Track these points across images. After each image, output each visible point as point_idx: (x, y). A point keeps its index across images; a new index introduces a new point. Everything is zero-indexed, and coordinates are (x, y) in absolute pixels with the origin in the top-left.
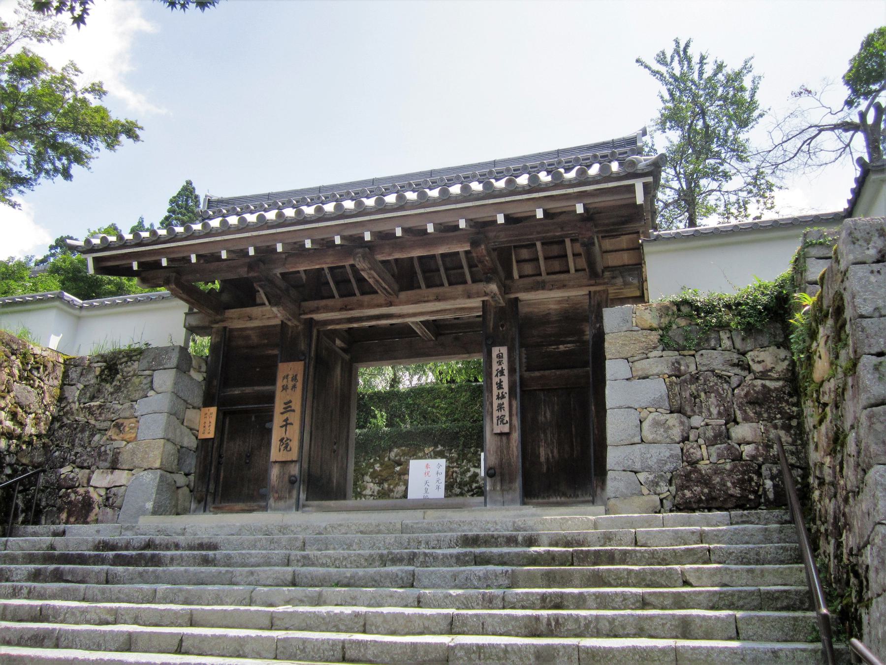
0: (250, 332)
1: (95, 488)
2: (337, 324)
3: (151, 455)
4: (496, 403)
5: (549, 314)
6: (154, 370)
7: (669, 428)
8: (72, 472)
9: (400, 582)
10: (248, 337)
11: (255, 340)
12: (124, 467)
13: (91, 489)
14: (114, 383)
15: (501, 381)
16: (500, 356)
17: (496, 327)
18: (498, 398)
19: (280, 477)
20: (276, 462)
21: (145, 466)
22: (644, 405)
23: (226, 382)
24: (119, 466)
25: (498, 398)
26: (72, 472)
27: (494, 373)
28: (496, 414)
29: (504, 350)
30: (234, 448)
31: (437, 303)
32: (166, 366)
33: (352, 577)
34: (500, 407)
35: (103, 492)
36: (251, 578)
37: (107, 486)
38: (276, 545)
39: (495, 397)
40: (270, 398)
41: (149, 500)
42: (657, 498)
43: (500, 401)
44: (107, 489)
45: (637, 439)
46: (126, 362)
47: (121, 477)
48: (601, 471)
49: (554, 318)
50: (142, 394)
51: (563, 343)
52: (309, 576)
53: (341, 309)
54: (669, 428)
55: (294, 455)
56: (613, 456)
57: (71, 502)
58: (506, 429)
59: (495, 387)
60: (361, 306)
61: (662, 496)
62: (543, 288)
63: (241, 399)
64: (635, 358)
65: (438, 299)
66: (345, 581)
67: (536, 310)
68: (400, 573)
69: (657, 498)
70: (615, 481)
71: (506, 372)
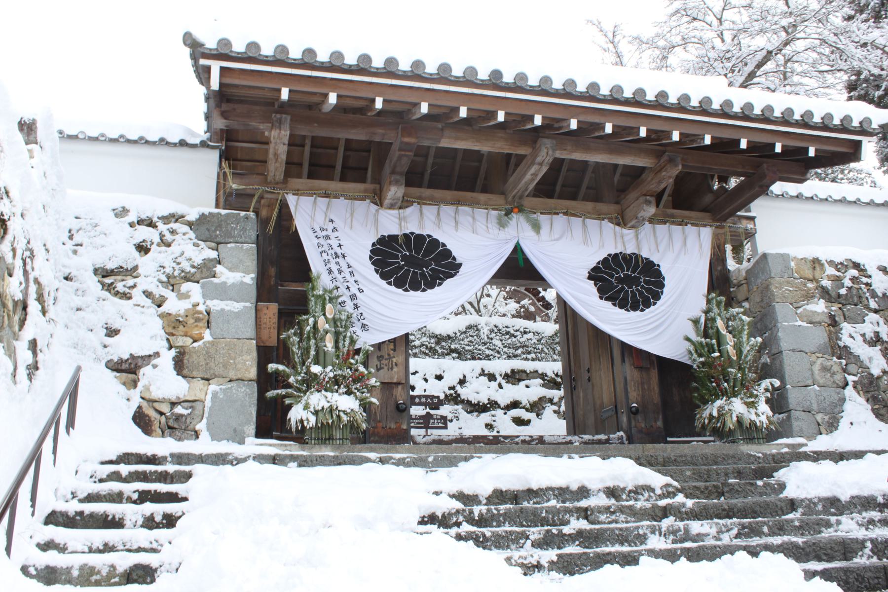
6: (218, 243)
21: (232, 374)
41: (248, 423)
54: (834, 373)
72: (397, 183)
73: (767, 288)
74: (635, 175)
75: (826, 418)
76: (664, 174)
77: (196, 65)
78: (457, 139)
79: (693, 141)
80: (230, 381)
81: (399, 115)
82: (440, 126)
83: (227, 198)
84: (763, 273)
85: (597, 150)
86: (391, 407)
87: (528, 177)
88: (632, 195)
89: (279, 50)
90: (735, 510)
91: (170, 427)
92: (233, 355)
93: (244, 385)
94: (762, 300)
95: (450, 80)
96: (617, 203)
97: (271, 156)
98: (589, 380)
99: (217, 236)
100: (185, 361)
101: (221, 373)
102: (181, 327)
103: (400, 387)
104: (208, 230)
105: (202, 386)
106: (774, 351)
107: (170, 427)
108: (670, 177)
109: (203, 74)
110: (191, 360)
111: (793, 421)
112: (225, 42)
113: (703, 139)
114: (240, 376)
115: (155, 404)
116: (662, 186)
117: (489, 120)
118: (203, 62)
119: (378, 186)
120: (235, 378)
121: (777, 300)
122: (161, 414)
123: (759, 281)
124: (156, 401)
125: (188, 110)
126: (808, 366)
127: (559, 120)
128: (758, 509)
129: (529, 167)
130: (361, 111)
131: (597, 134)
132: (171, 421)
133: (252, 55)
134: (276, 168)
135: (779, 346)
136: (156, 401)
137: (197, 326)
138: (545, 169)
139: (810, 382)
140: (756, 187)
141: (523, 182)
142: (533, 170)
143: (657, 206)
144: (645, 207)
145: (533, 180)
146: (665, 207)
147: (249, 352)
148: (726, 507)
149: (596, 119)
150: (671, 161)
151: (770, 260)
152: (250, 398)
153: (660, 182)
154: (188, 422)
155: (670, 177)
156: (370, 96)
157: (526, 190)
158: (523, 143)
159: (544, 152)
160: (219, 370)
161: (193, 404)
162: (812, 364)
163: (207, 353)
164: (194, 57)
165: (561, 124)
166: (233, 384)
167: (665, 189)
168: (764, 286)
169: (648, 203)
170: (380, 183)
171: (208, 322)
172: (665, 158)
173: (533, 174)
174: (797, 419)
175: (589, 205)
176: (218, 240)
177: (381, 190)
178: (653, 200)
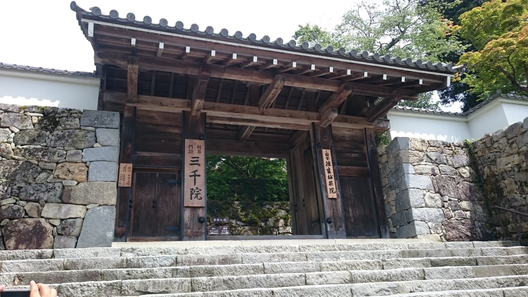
0: (154, 115)
1: (48, 219)
2: (221, 120)
3: (105, 193)
4: (328, 181)
5: (344, 136)
6: (96, 128)
7: (436, 200)
8: (15, 204)
9: (417, 277)
10: (152, 118)
11: (159, 121)
12: (77, 202)
13: (42, 220)
14: (55, 133)
15: (329, 169)
16: (327, 155)
17: (322, 139)
18: (329, 178)
19: (192, 218)
20: (188, 207)
21: (101, 202)
22: (424, 188)
23: (136, 148)
24: (72, 201)
25: (329, 178)
26: (15, 204)
27: (325, 164)
28: (329, 187)
29: (329, 151)
30: (147, 196)
31: (289, 119)
32: (109, 126)
33: (389, 275)
34: (331, 183)
35: (57, 223)
36: (321, 280)
37: (62, 217)
38: (286, 259)
39: (327, 178)
40: (181, 164)
41: (109, 230)
42: (438, 236)
43: (331, 180)
44: (62, 220)
45: (424, 205)
46: (67, 117)
47: (77, 211)
48: (410, 222)
49: (347, 139)
50: (87, 144)
51: (354, 153)
52: (361, 276)
53: (230, 111)
54: (436, 200)
55: (202, 203)
56: (416, 212)
57: (20, 231)
58: (335, 196)
59: (326, 172)
60: (243, 111)
61: (441, 235)
62: (347, 122)
63: (149, 160)
64: (415, 164)
65: (291, 116)
66: (385, 278)
67: (338, 133)
68: (416, 271)
69: (438, 236)
70: (419, 227)
71: (331, 164)
72: (200, 98)
73: (398, 155)
74: (325, 97)
75: (434, 225)
76: (342, 94)
77: (80, 23)
78: (232, 74)
79: (357, 76)
80: (99, 206)
81: (202, 63)
82: (223, 67)
83: (102, 105)
84: (395, 148)
85: (307, 82)
86: (196, 220)
87: (271, 96)
88: (325, 108)
89: (129, 16)
90: (392, 275)
91: (59, 234)
92: (102, 190)
93: (108, 208)
94: (395, 162)
95: (227, 39)
96: (317, 112)
97: (128, 80)
98: (304, 205)
99: (95, 124)
100: (72, 194)
101: (94, 201)
102: (70, 175)
103: (201, 209)
104: (90, 120)
105: (81, 209)
106: (403, 188)
107: (59, 234)
108: (345, 96)
109: (84, 28)
110: (75, 194)
111: (416, 226)
112: (96, 9)
113: (364, 74)
114: (105, 203)
115: (50, 221)
116: (342, 101)
117: (249, 62)
118: (83, 20)
119: (190, 101)
120: (102, 204)
121: (404, 161)
122: (54, 226)
123: (393, 151)
124: (51, 219)
125: (83, 58)
126: (422, 196)
127: (286, 63)
128: (404, 275)
129: (271, 90)
130: (180, 57)
131: (307, 71)
132: (60, 230)
133: (113, 17)
134: (132, 89)
135: (406, 185)
136: (51, 219)
137: (80, 174)
138: (279, 91)
139: (424, 205)
140: (389, 104)
141: (268, 99)
142: (273, 91)
143: (339, 114)
144: (332, 113)
145: (273, 97)
146: (343, 114)
147: (112, 188)
148: (386, 274)
149: (306, 63)
150: (347, 88)
151: (399, 140)
152: (111, 215)
153: (340, 99)
154: (71, 231)
155: (345, 96)
156: (183, 46)
157: (270, 103)
158: (267, 77)
159: (278, 82)
160: (91, 199)
161: (75, 220)
162: (424, 195)
163: (86, 189)
164: (78, 18)
165: (287, 66)
166: (101, 207)
167: (343, 103)
168: (396, 154)
169: (334, 111)
170: (190, 98)
171: (88, 172)
172: (343, 86)
173: (274, 94)
174: (418, 225)
175: (303, 113)
176: (96, 126)
177: (192, 102)
178: (337, 110)
